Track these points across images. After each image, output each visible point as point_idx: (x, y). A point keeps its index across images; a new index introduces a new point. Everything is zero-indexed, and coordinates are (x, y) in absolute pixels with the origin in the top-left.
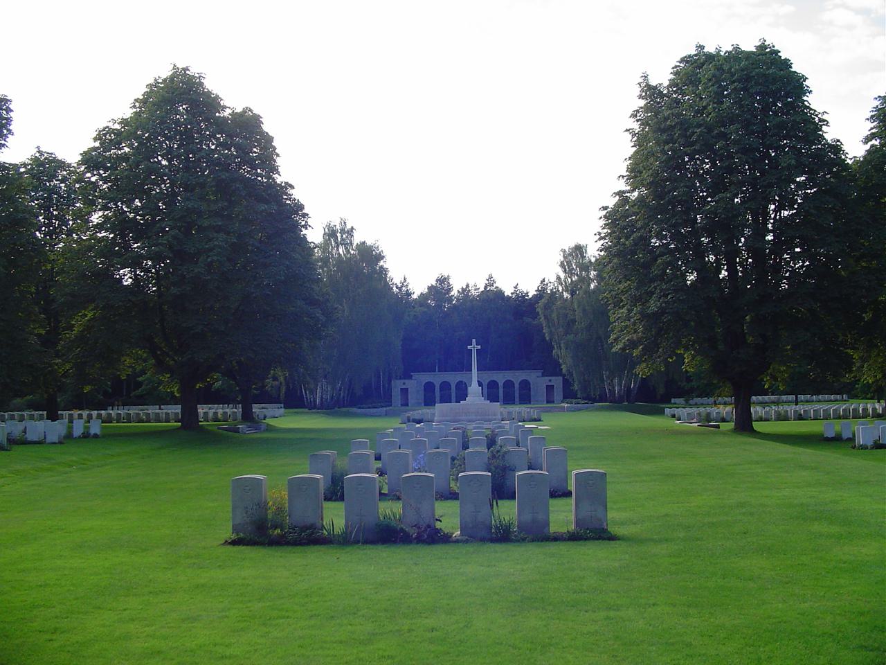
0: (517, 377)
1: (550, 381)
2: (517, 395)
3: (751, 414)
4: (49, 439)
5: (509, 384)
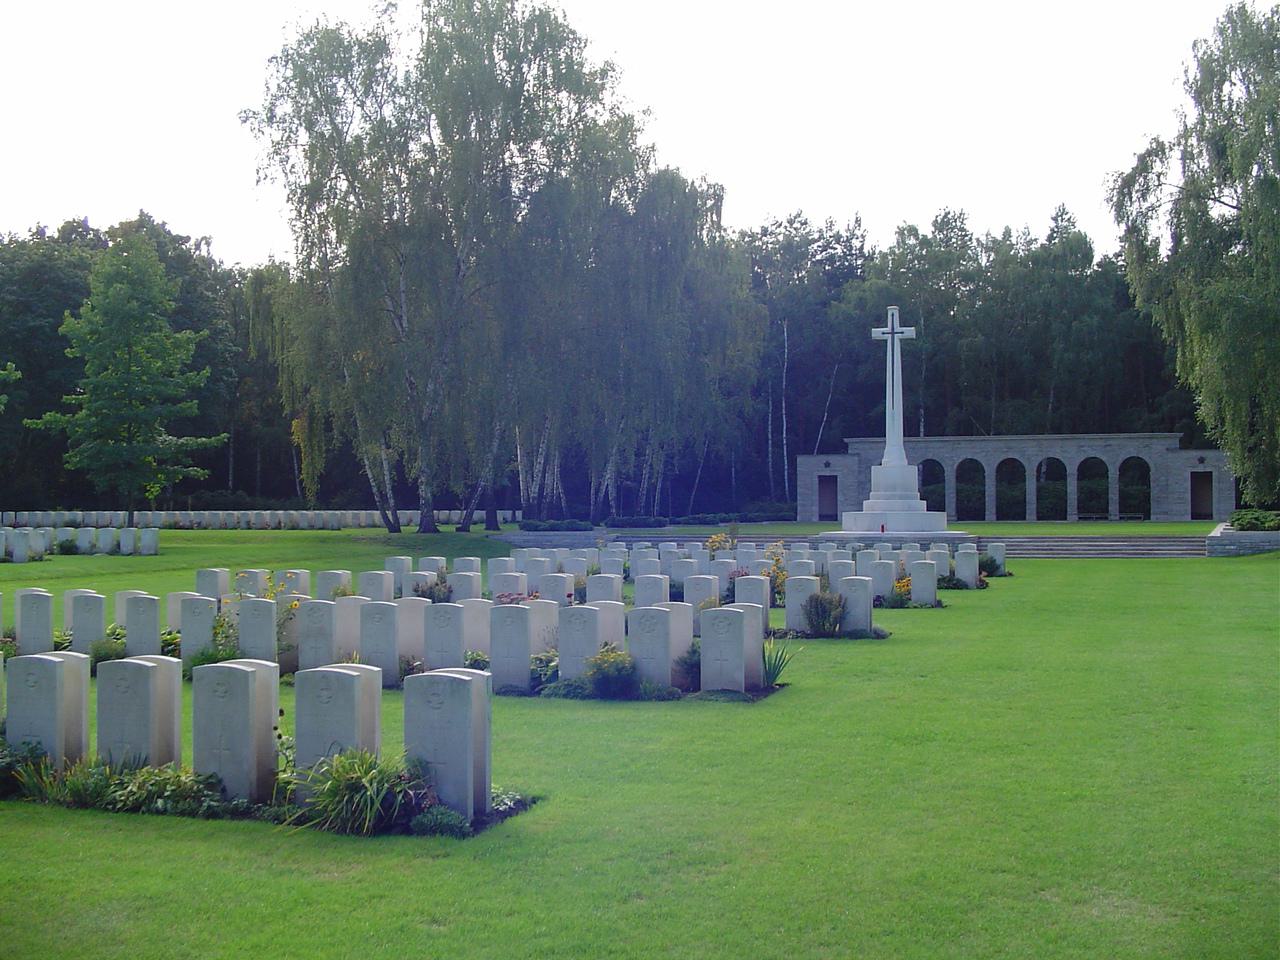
0: (1113, 450)
1: (1202, 460)
2: (1114, 496)
3: (204, 510)
4: (124, 549)
5: (1011, 471)
